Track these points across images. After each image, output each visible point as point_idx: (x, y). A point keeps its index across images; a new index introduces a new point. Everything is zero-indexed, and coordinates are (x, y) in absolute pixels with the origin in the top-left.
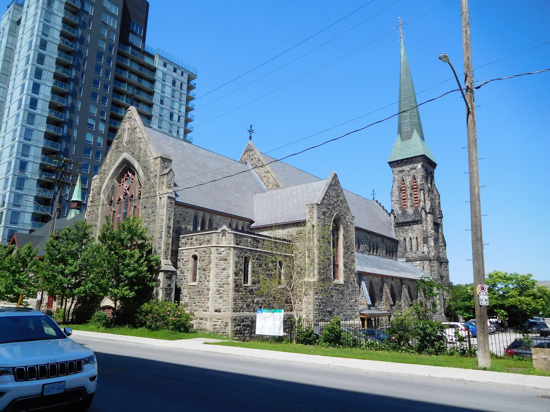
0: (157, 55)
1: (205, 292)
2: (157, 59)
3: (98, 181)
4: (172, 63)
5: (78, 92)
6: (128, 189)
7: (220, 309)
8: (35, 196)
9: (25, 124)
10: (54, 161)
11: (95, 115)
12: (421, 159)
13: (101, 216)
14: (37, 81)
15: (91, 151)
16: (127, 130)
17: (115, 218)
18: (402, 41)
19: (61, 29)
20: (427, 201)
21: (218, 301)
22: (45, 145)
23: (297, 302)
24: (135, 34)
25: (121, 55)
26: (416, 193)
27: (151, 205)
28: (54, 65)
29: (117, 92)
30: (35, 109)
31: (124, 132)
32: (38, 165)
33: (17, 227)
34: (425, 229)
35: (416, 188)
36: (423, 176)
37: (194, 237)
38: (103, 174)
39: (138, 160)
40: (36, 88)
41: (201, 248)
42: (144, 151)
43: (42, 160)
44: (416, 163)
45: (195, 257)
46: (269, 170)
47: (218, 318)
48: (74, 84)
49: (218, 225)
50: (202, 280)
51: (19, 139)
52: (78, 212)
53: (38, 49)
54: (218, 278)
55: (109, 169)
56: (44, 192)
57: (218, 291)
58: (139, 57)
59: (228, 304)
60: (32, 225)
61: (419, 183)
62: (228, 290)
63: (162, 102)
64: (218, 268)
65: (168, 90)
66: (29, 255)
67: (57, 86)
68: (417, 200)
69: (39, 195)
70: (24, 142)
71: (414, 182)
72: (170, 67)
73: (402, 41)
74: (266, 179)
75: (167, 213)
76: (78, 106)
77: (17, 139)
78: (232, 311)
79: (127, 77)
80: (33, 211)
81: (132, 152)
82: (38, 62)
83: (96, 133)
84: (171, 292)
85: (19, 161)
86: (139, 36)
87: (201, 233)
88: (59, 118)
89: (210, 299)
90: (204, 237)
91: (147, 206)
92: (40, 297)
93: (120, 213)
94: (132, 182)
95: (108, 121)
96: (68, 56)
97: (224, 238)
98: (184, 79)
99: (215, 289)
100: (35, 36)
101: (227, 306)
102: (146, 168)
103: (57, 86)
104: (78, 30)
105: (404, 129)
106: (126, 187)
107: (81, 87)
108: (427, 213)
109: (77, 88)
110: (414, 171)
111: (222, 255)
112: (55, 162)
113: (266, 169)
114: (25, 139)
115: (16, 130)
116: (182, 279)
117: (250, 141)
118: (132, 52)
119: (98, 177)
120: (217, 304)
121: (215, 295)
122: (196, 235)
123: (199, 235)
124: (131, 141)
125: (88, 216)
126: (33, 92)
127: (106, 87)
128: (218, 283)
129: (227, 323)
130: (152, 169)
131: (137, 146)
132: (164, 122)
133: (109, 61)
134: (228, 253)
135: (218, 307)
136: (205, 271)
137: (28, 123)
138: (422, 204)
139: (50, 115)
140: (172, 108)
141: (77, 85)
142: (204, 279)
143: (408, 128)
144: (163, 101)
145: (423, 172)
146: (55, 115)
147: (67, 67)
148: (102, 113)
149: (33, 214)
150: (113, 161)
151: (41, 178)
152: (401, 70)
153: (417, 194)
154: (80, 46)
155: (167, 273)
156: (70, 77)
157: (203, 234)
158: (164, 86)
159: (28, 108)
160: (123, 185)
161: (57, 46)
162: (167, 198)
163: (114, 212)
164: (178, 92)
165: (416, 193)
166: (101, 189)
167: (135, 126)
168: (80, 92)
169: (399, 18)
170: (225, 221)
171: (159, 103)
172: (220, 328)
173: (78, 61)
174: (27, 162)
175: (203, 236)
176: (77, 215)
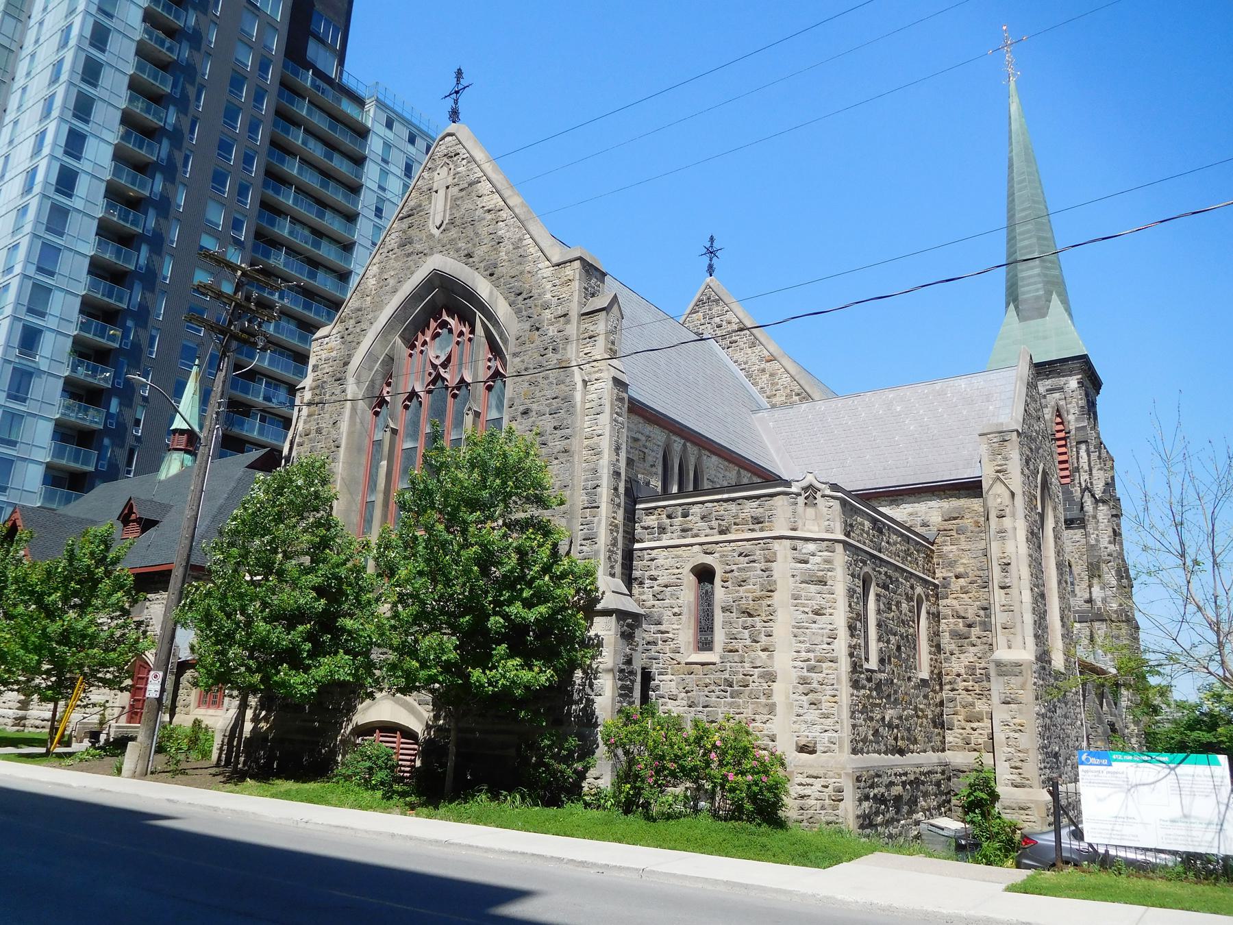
0: (373, 99)
1: (756, 684)
2: (371, 108)
3: (334, 342)
4: (406, 122)
5: (179, 164)
6: (445, 365)
7: (815, 743)
8: (56, 420)
9: (41, 232)
10: (111, 332)
12: (1077, 365)
13: (347, 444)
14: (79, 125)
16: (442, 192)
17: (398, 452)
18: (1012, 84)
19: (146, 5)
20: (1094, 472)
21: (808, 717)
22: (89, 290)
23: (956, 723)
24: (322, 41)
25: (289, 88)
26: (1063, 450)
27: (549, 405)
28: (124, 92)
30: (70, 196)
31: (430, 199)
32: (69, 342)
34: (1093, 542)
35: (1064, 439)
36: (1082, 407)
37: (695, 509)
38: (352, 322)
39: (488, 273)
40: (75, 143)
41: (730, 542)
42: (511, 247)
43: (81, 329)
44: (1063, 376)
45: (704, 574)
46: (775, 354)
47: (810, 772)
48: (171, 145)
50: (736, 645)
51: (25, 268)
52: (188, 458)
53: (86, 46)
54: (802, 639)
55: (378, 306)
56: (79, 411)
57: (804, 681)
58: (329, 97)
59: (838, 727)
60: (44, 498)
61: (1072, 426)
62: (835, 682)
63: (379, 212)
64: (802, 609)
66: (101, 561)
68: (1067, 469)
69: (67, 418)
71: (1057, 424)
72: (402, 131)
73: (1012, 84)
74: (765, 377)
75: (612, 429)
77: (18, 269)
78: (850, 750)
79: (300, 142)
80: (48, 460)
81: (463, 253)
82: (83, 80)
84: (633, 682)
86: (331, 47)
87: (725, 496)
88: (128, 225)
89: (779, 709)
90: (739, 507)
91: (534, 407)
92: (158, 687)
93: (414, 435)
94: (458, 343)
95: (249, 245)
96: (161, 72)
97: (810, 511)
99: (794, 675)
100: (81, 15)
101: (835, 734)
102: (521, 297)
103: (130, 143)
104: (187, 13)
105: (1024, 293)
106: (437, 357)
107: (188, 152)
108: (1097, 501)
109: (179, 157)
110: (1057, 395)
111: (808, 566)
112: (113, 335)
113: (765, 351)
114: (40, 269)
115: (16, 246)
116: (655, 643)
117: (708, 279)
118: (313, 81)
119: (334, 331)
120: (804, 726)
121: (796, 696)
122: (703, 503)
123: (717, 501)
124: (458, 222)
125: (300, 445)
126: (66, 153)
127: (248, 160)
128: (804, 655)
129: (840, 790)
130: (548, 296)
131: (483, 231)
133: (258, 97)
134: (827, 561)
135: (808, 734)
136: (750, 615)
137: (48, 229)
138: (1085, 476)
139: (107, 216)
141: (179, 149)
142: (748, 642)
143: (1037, 290)
144: (382, 210)
145: (1081, 399)
146: (119, 218)
147: (156, 99)
148: (237, 225)
149: (49, 467)
150: (392, 282)
151: (74, 375)
152: (1011, 151)
153: (1065, 453)
154: (143, 294)
155: (624, 620)
156: (162, 124)
157: (733, 500)
158: (384, 173)
159: (51, 192)
160: (422, 352)
162: (611, 383)
163: (394, 432)
165: (1063, 450)
166: (346, 364)
167: (473, 178)
168: (186, 165)
169: (1004, 28)
170: (727, 474)
171: (372, 215)
172: (818, 807)
173: (183, 89)
174: (41, 331)
175: (733, 507)
176: (187, 467)
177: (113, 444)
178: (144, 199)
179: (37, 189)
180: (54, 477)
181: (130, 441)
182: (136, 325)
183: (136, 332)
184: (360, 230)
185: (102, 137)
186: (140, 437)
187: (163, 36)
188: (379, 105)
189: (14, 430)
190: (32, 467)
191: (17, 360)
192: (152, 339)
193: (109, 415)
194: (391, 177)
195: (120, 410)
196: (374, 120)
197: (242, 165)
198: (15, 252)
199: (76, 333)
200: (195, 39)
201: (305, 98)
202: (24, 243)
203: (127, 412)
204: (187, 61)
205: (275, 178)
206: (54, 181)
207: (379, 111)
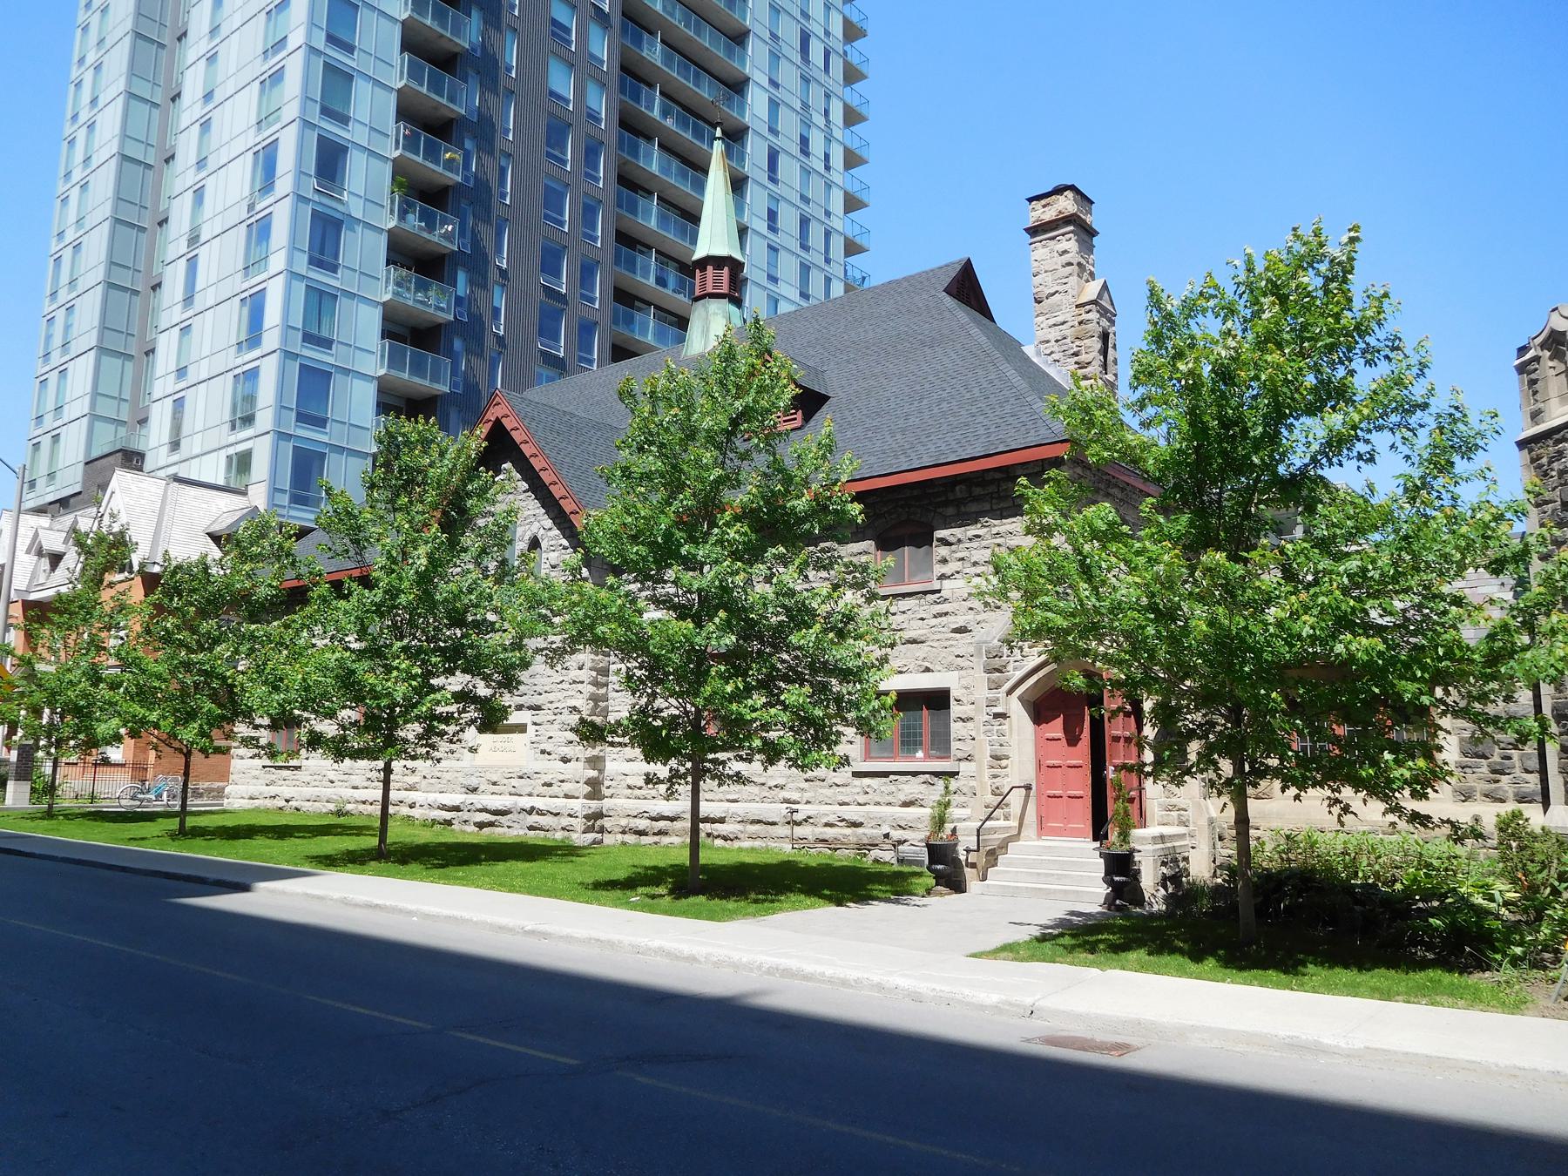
5: (494, 184)
10: (447, 156)
29: (631, 183)
76: (508, 60)
79: (652, 281)
83: (582, 64)
85: (288, 449)
115: (277, 77)
140: (805, 199)
154: (482, 94)
164: (819, 88)
178: (441, 396)
181: (490, 342)
186: (506, 270)
190: (358, 384)
191: (316, 198)
192: (503, 171)
195: (472, 291)
197: (582, 229)
198: (281, 17)
199: (397, 154)
200: (486, 67)
201: (653, 139)
206: (287, 485)
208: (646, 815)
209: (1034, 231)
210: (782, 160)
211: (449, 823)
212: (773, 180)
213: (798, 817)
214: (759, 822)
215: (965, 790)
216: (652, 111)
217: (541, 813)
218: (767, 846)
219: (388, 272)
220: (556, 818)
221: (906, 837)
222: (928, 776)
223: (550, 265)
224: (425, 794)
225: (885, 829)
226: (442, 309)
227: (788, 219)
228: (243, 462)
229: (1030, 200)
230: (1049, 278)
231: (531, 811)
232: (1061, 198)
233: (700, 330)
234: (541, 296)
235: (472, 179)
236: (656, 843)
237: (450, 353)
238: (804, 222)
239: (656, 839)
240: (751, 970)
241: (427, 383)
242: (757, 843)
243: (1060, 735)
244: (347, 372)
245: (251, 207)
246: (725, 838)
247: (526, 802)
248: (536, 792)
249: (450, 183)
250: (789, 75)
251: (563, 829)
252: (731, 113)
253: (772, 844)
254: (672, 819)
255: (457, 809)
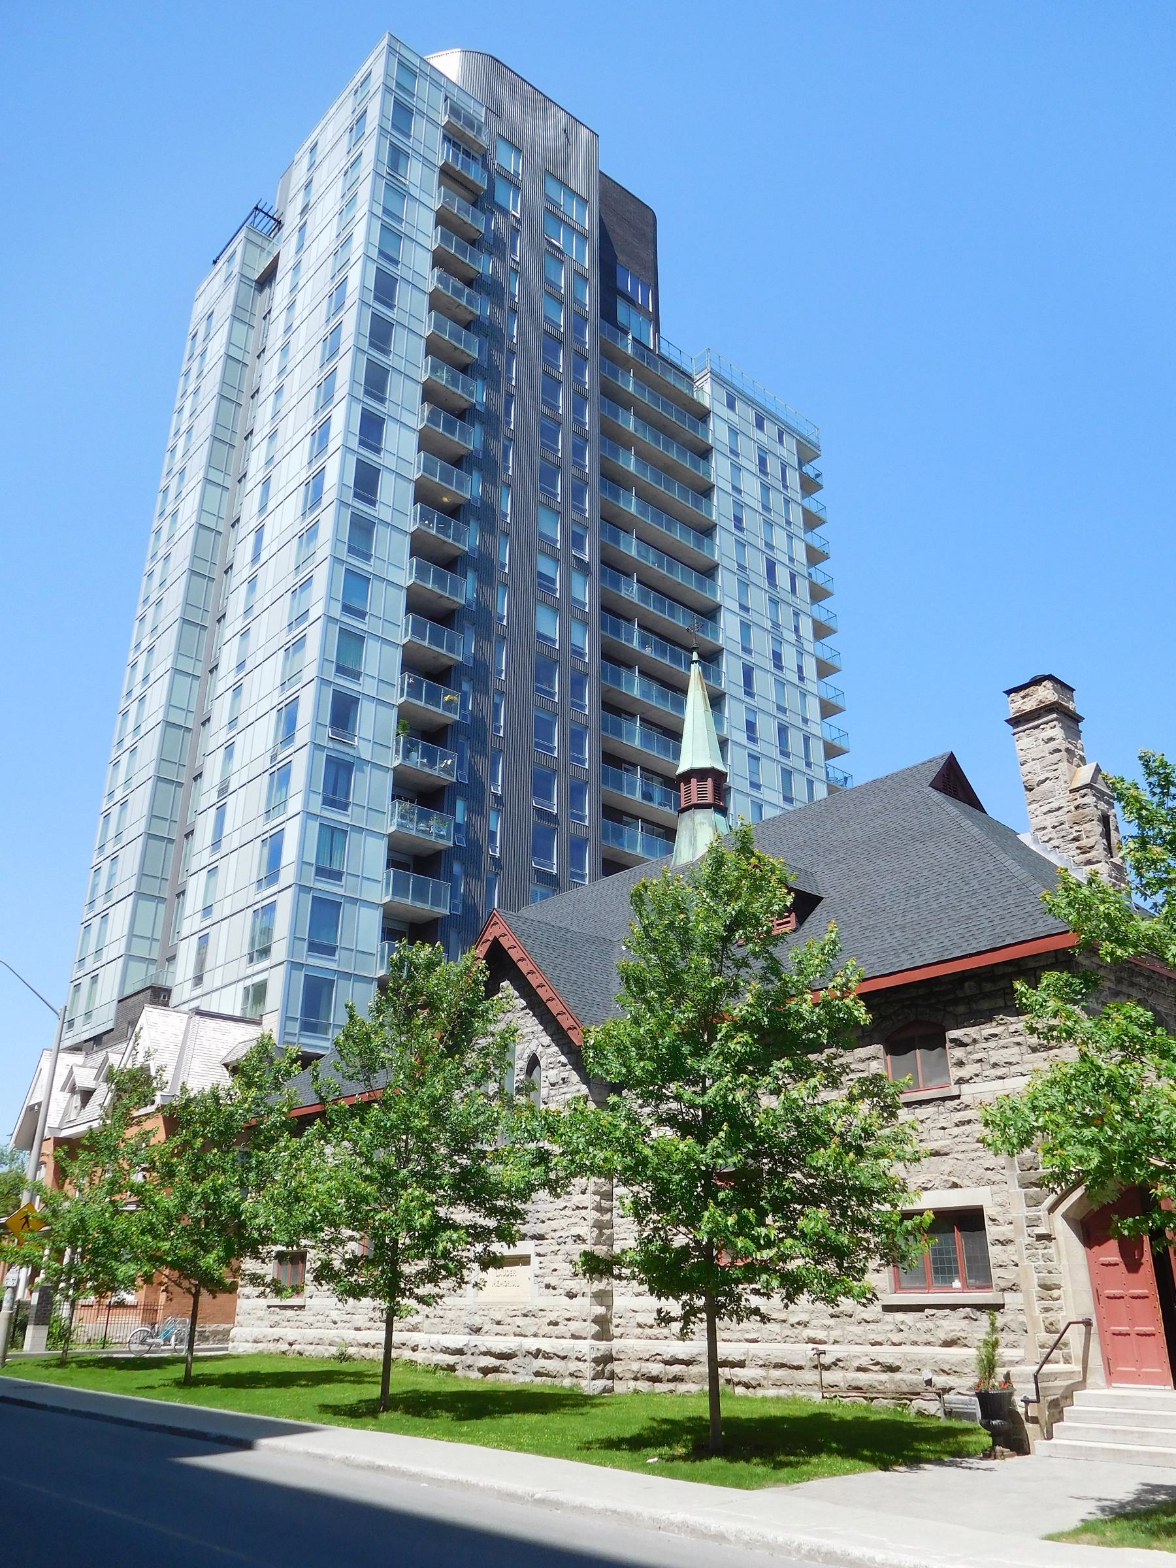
0: (706, 371)
4: (750, 402)
5: (489, 720)
8: (390, 835)
10: (447, 698)
11: (554, 641)
15: (551, 783)
33: (334, 966)
49: (1000, 1319)
65: (751, 485)
67: (437, 429)
70: (326, 814)
79: (638, 796)
83: (566, 609)
98: (788, 450)
100: (344, 404)
109: (496, 447)
112: (450, 702)
114: (347, 609)
126: (362, 443)
132: (752, 590)
148: (578, 542)
151: (407, 763)
161: (407, 542)
168: (496, 717)
171: (731, 526)
173: (490, 356)
177: (467, 874)
179: (287, 875)
180: (399, 858)
181: (487, 865)
182: (474, 690)
183: (475, 698)
184: (713, 431)
185: (402, 420)
186: (501, 797)
187: (460, 285)
188: (716, 379)
189: (336, 856)
191: (330, 745)
192: (496, 708)
193: (458, 827)
194: (744, 473)
195: (470, 819)
196: (713, 398)
202: (321, 577)
203: (477, 821)
204: (480, 552)
205: (613, 479)
207: (716, 386)
208: (658, 1357)
209: (1016, 721)
210: (757, 675)
211: (452, 1368)
212: (749, 693)
213: (826, 1360)
214: (783, 1366)
215: (1013, 1326)
216: (631, 641)
217: (547, 1356)
218: (794, 1395)
219: (394, 806)
220: (563, 1363)
221: (952, 1384)
222: (968, 1309)
223: (542, 789)
224: (428, 1336)
225: (927, 1374)
226: (442, 837)
227: (767, 729)
228: (258, 993)
229: (1009, 692)
230: (1037, 766)
231: (537, 1354)
232: (1040, 688)
233: (687, 843)
234: (534, 817)
235: (469, 717)
236: (671, 1391)
237: (451, 878)
238: (783, 730)
239: (671, 1386)
240: (789, 1553)
241: (428, 907)
242: (783, 1392)
243: (1117, 1259)
244: (354, 901)
245: (273, 758)
246: (747, 1386)
247: (532, 1344)
248: (541, 1333)
249: (449, 722)
250: (758, 599)
251: (571, 1375)
252: (706, 637)
253: (800, 1393)
254: (688, 1363)
255: (460, 1352)
